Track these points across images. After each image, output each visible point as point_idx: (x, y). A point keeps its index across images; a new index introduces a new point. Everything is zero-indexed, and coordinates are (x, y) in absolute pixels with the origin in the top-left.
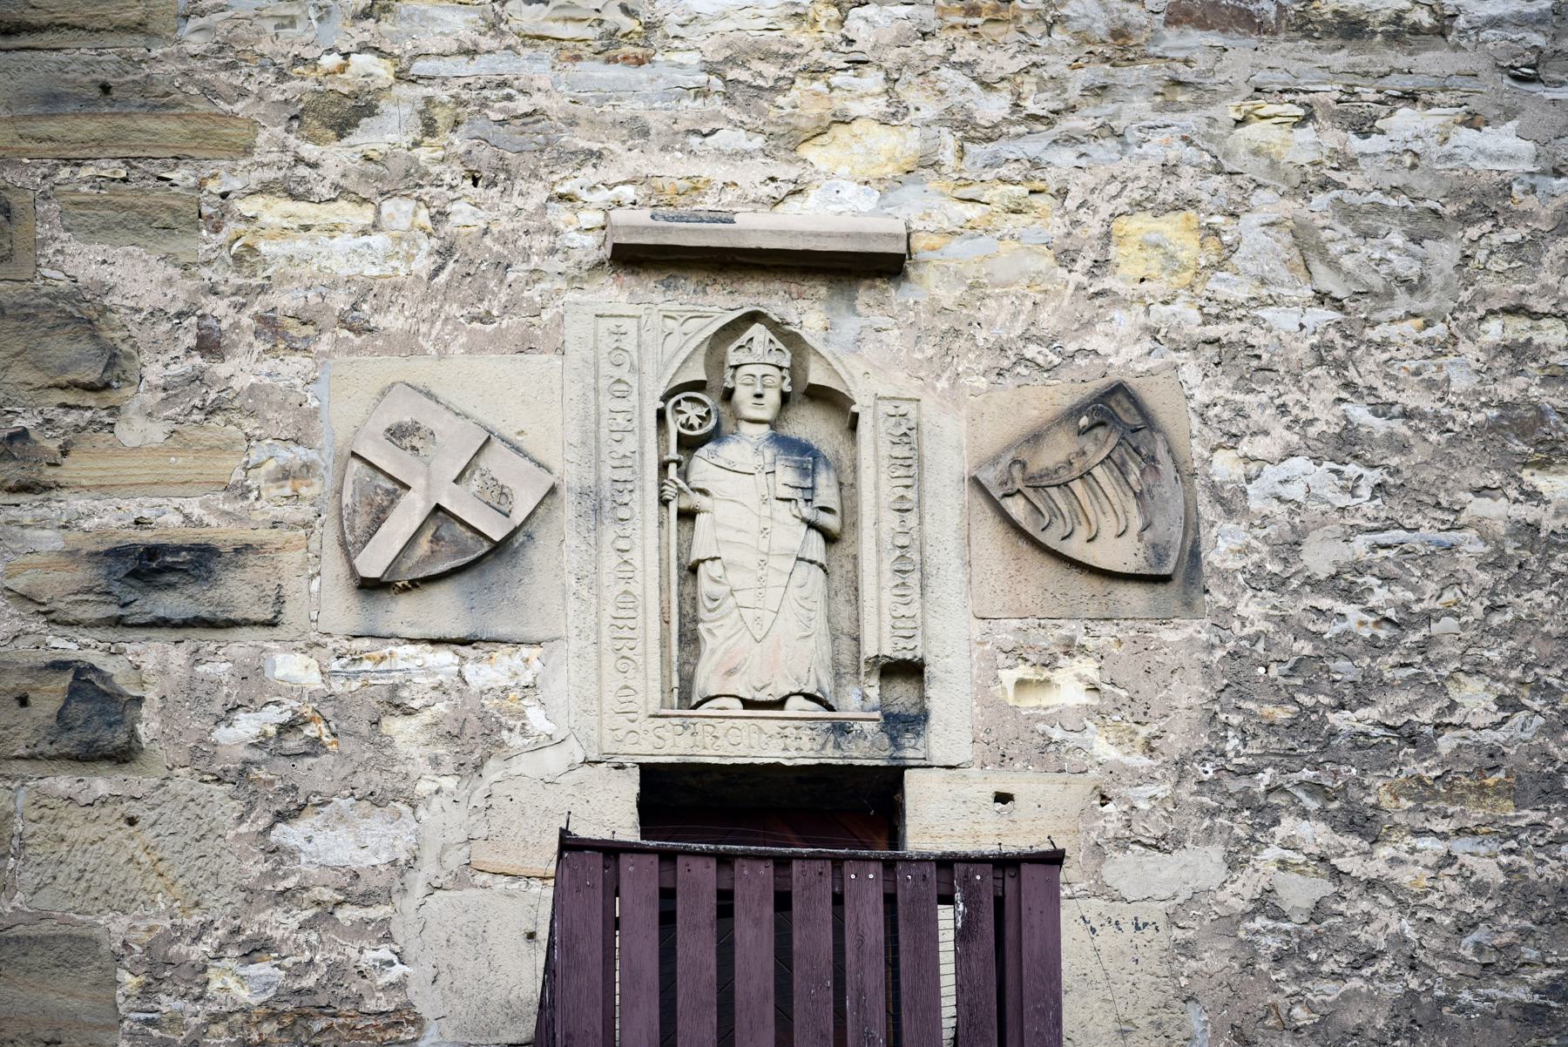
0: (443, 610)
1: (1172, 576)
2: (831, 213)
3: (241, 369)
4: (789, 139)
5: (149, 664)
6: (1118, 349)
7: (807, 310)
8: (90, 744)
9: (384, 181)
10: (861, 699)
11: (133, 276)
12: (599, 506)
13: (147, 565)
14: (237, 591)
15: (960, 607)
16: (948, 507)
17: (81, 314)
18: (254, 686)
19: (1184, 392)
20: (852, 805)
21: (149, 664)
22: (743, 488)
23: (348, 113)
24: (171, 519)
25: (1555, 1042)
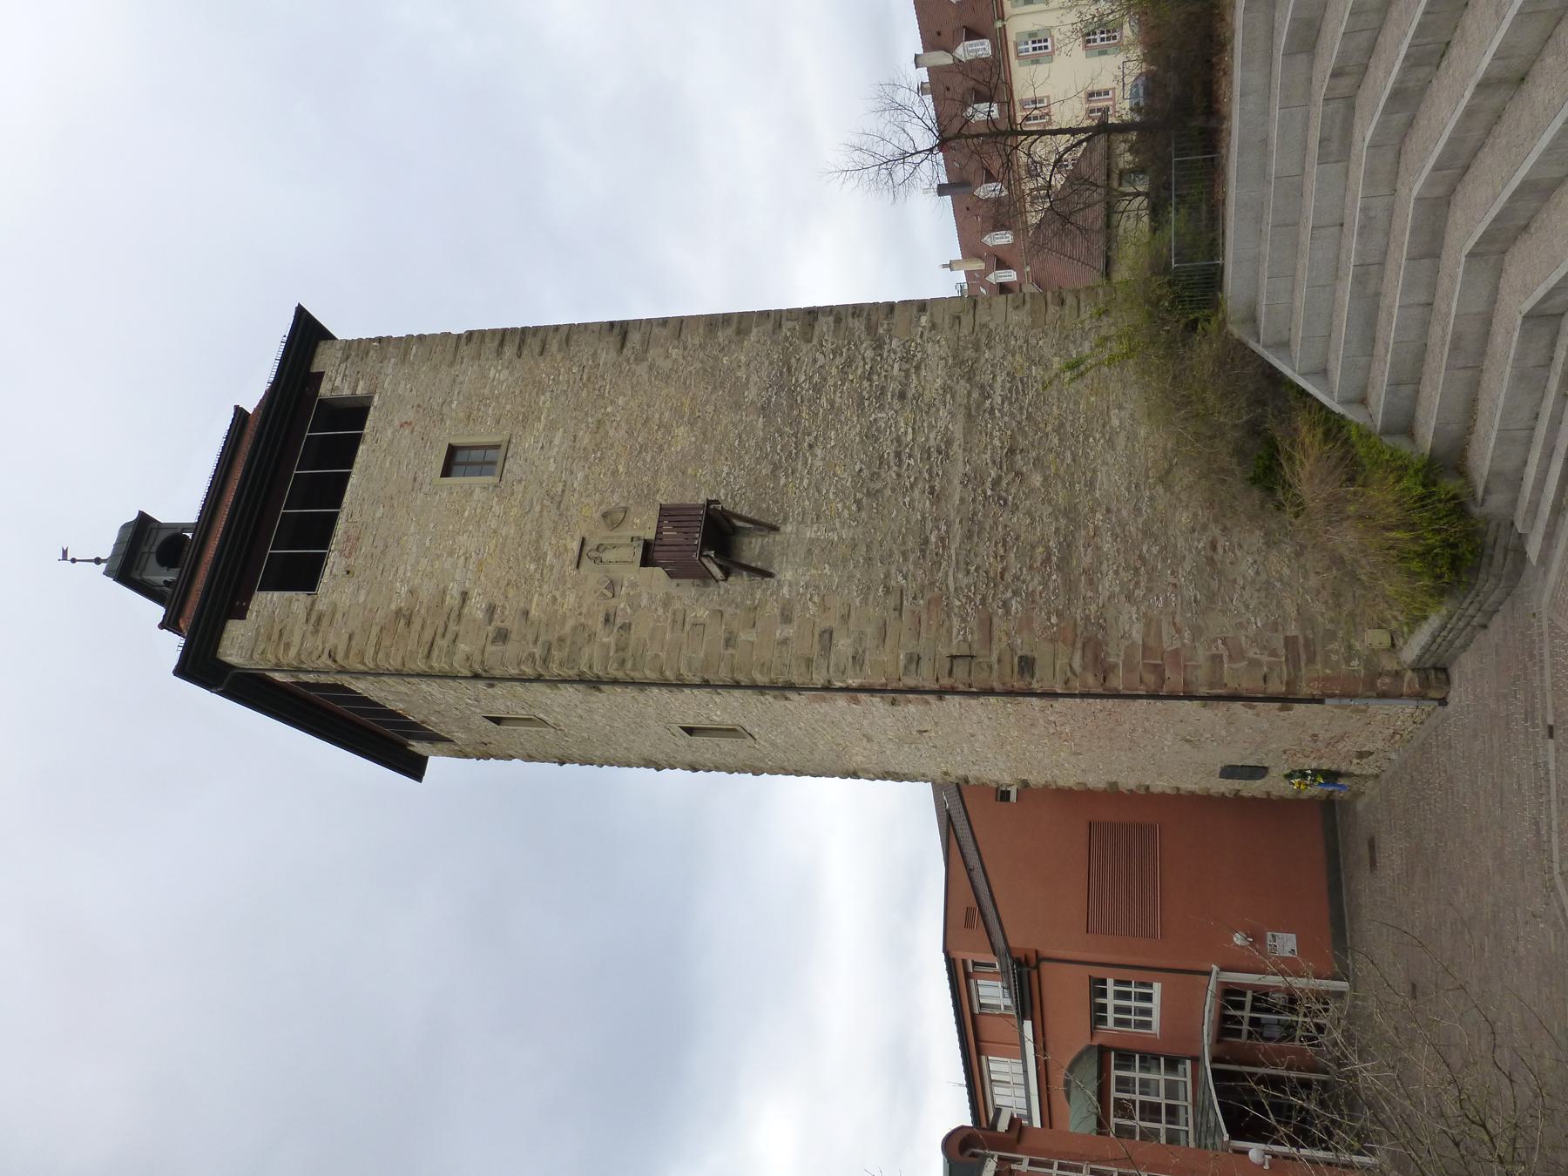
0: (617, 589)
1: (626, 510)
2: (575, 546)
3: (584, 611)
4: (566, 550)
5: (619, 621)
6: (597, 516)
7: (587, 548)
8: (492, 686)
9: (563, 594)
10: (635, 543)
11: (570, 623)
12: (607, 571)
13: (607, 620)
14: (612, 611)
15: (627, 532)
16: (613, 533)
17: (575, 629)
18: (624, 609)
19: (604, 508)
20: (647, 546)
21: (619, 621)
22: (606, 556)
23: (554, 599)
24: (601, 618)
25: (1024, 1167)
